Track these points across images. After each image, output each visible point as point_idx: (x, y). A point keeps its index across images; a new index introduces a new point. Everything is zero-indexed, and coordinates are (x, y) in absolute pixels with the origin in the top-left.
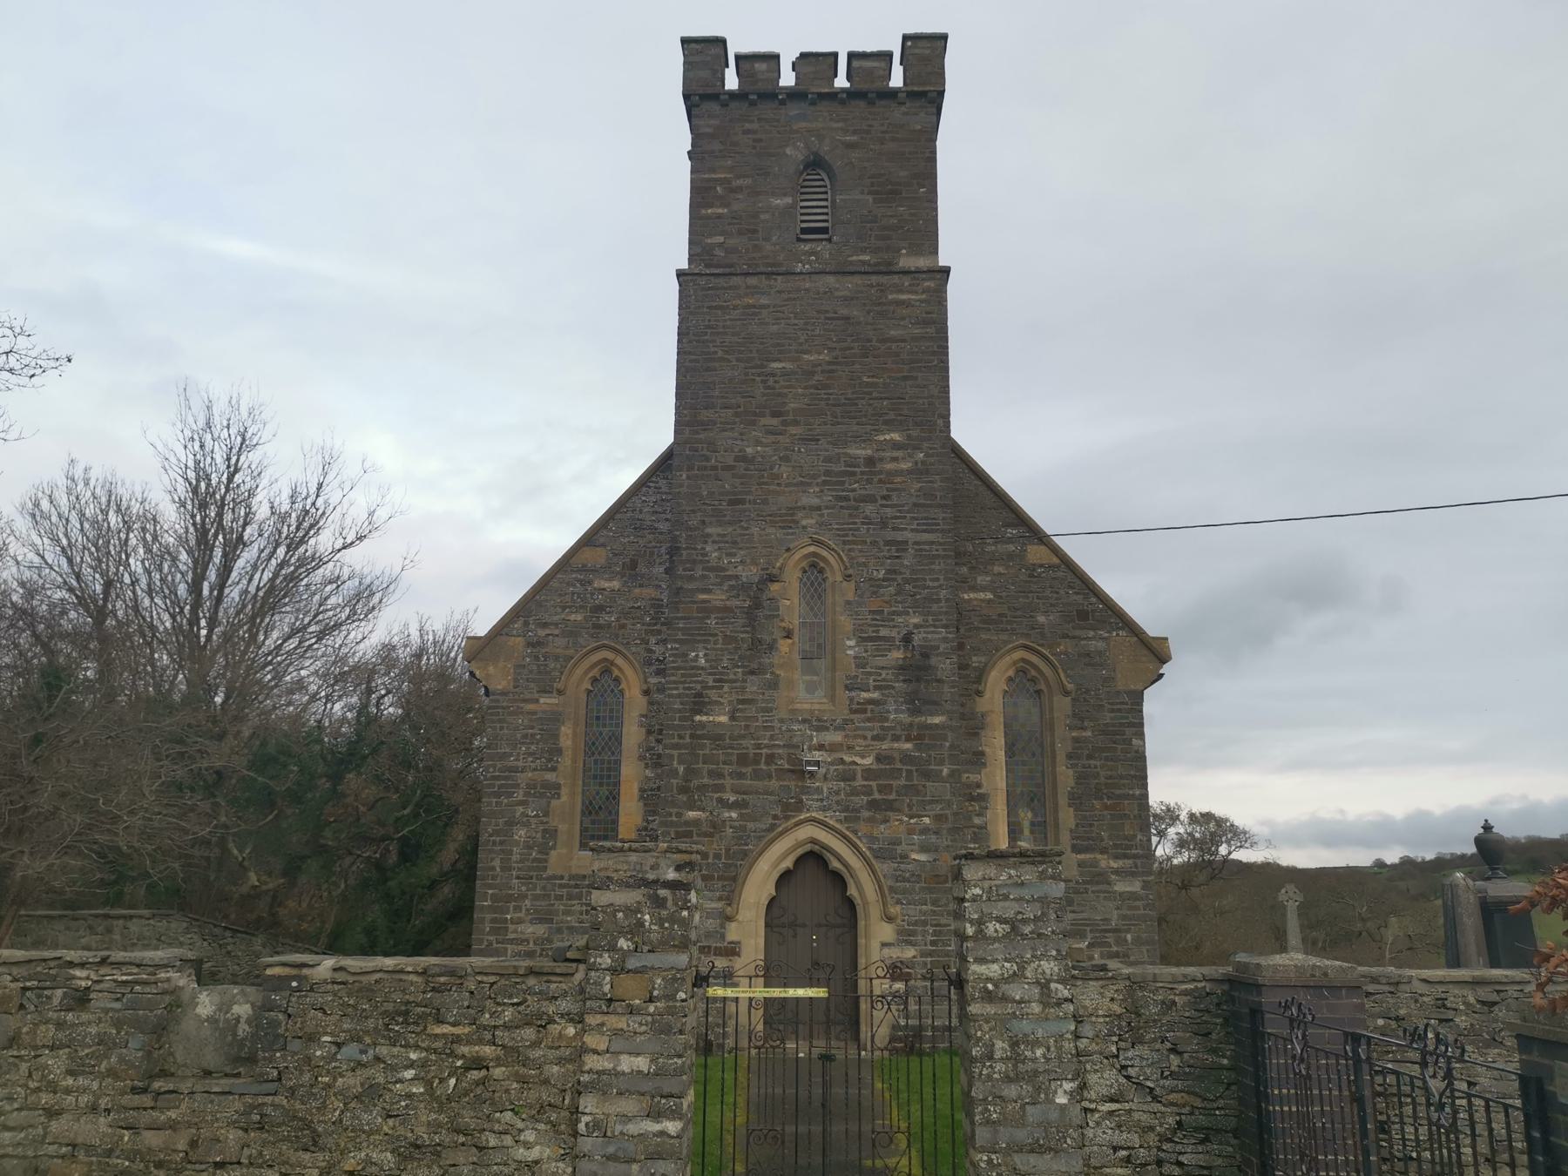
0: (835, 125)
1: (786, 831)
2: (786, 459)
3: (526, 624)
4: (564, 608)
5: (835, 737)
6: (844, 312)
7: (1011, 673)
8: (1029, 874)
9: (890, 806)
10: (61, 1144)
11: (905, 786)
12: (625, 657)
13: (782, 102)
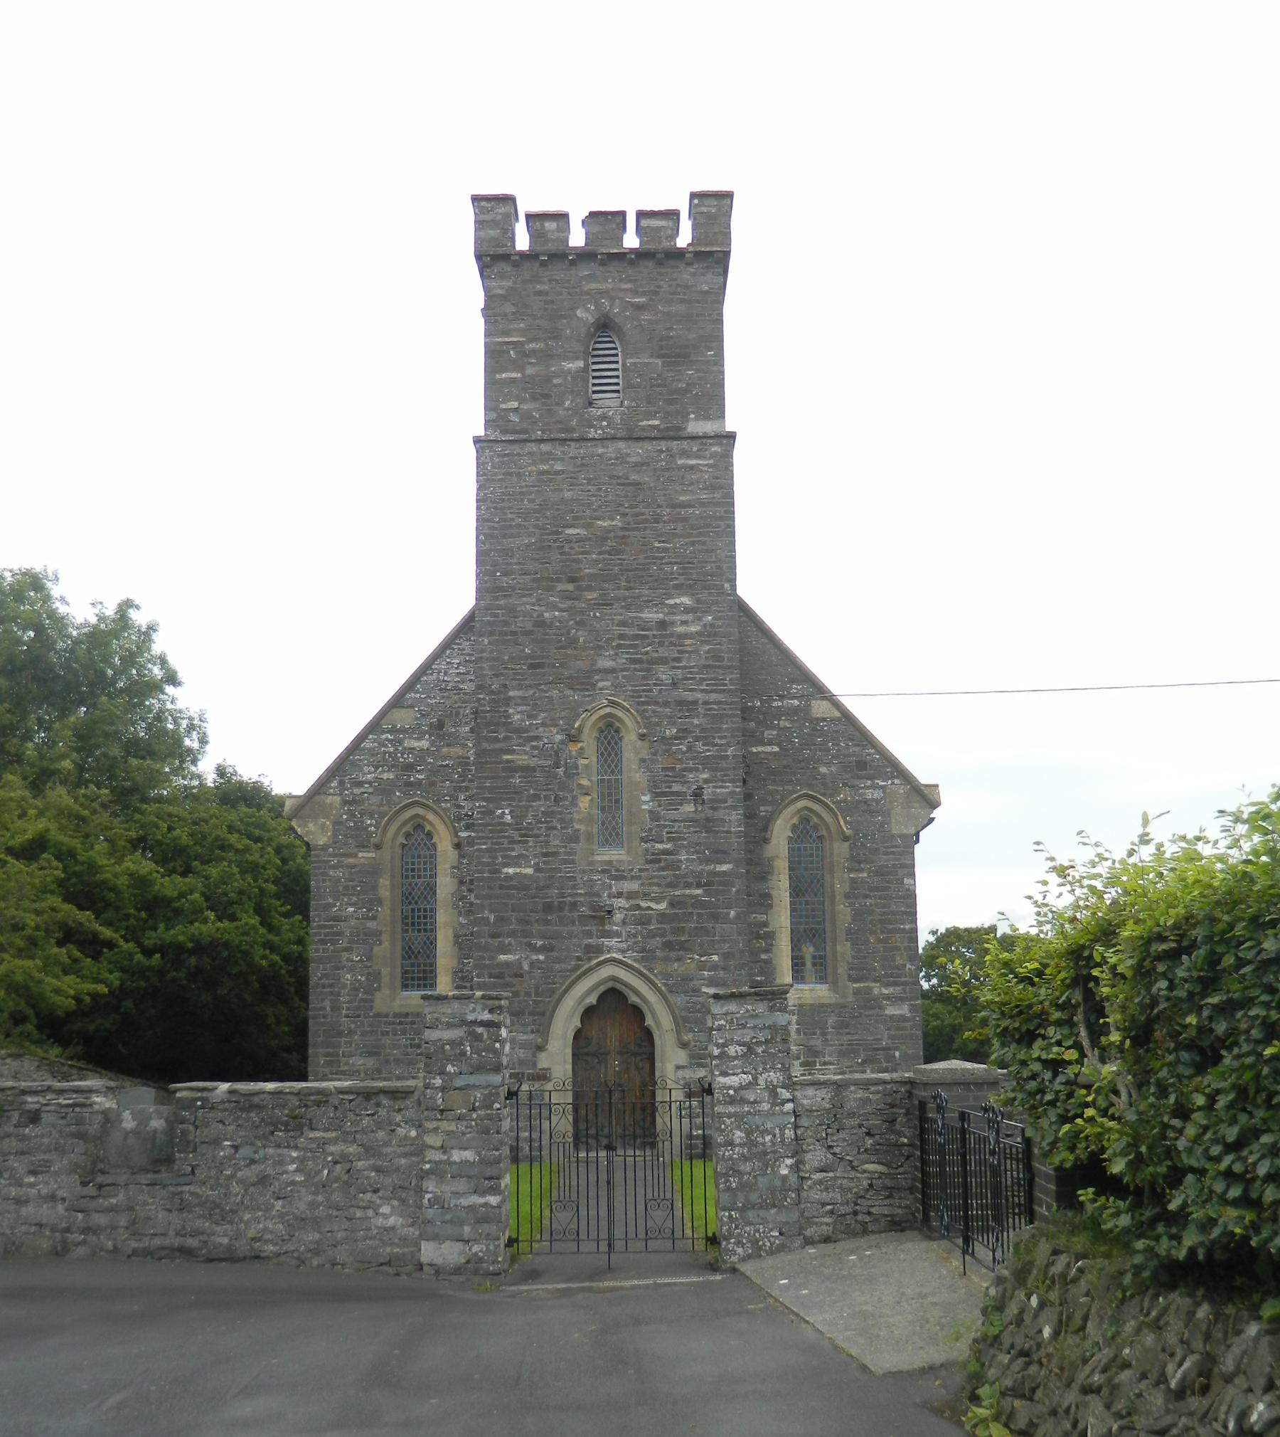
0: (625, 286)
1: (590, 969)
2: (581, 624)
3: (342, 783)
4: (376, 768)
5: (634, 886)
6: (634, 477)
7: (795, 820)
8: (761, 1008)
9: (683, 946)
10: (31, 1225)
11: (696, 928)
12: (436, 813)
13: (573, 263)
